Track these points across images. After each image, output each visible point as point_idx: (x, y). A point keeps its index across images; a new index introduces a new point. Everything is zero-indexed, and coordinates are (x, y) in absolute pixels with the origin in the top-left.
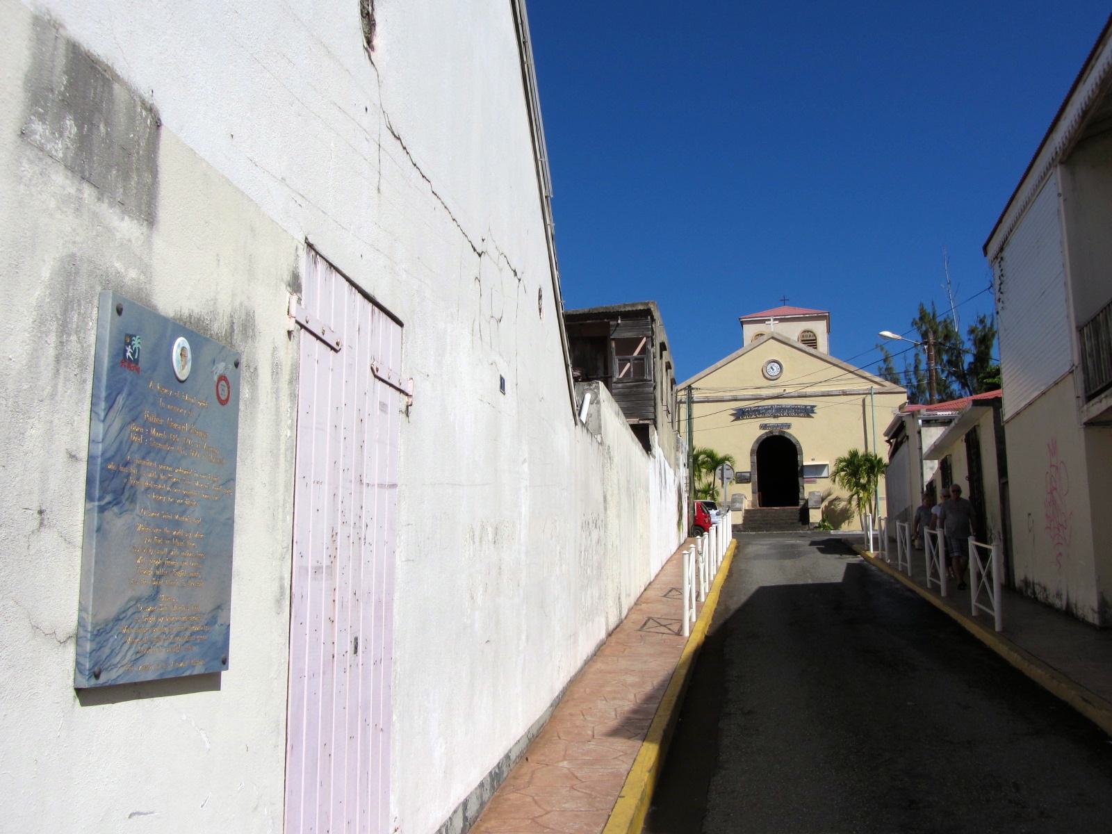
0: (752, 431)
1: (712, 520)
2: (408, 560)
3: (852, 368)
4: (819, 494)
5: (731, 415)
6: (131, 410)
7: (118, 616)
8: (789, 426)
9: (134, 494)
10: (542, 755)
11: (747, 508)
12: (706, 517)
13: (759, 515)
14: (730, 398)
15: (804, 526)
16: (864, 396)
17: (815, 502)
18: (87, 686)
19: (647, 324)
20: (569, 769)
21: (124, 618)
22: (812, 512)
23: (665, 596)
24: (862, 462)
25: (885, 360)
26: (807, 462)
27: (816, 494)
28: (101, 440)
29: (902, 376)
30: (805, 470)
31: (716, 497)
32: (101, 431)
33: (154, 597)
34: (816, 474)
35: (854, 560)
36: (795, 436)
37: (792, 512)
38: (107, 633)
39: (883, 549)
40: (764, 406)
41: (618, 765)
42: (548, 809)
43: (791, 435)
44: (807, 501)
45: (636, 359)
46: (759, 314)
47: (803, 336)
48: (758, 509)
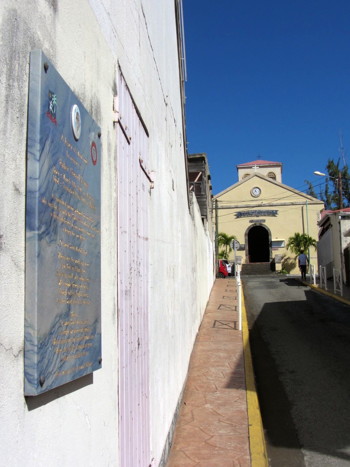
0: (246, 224)
1: (227, 269)
2: (151, 287)
3: (297, 191)
4: (280, 256)
5: (234, 215)
6: (53, 155)
7: (51, 331)
8: (264, 221)
9: (57, 226)
10: (193, 400)
11: (243, 263)
12: (224, 268)
13: (250, 267)
14: (234, 207)
15: (273, 272)
16: (303, 205)
17: (278, 260)
18: (36, 394)
19: (203, 165)
20: (212, 409)
21: (54, 332)
22: (277, 265)
23: (218, 309)
24: (302, 239)
25: (310, 188)
26: (273, 239)
27: (279, 256)
28: (38, 177)
29: (319, 195)
30: (273, 243)
31: (227, 257)
32: (38, 169)
33: (67, 315)
34: (279, 246)
35: (308, 288)
36: (267, 226)
37: (266, 265)
38: (46, 346)
39: (323, 283)
40: (251, 211)
41: (239, 405)
42: (211, 434)
43: (265, 226)
44: (274, 260)
45: (196, 184)
46: (243, 165)
47: (269, 175)
48: (249, 264)
